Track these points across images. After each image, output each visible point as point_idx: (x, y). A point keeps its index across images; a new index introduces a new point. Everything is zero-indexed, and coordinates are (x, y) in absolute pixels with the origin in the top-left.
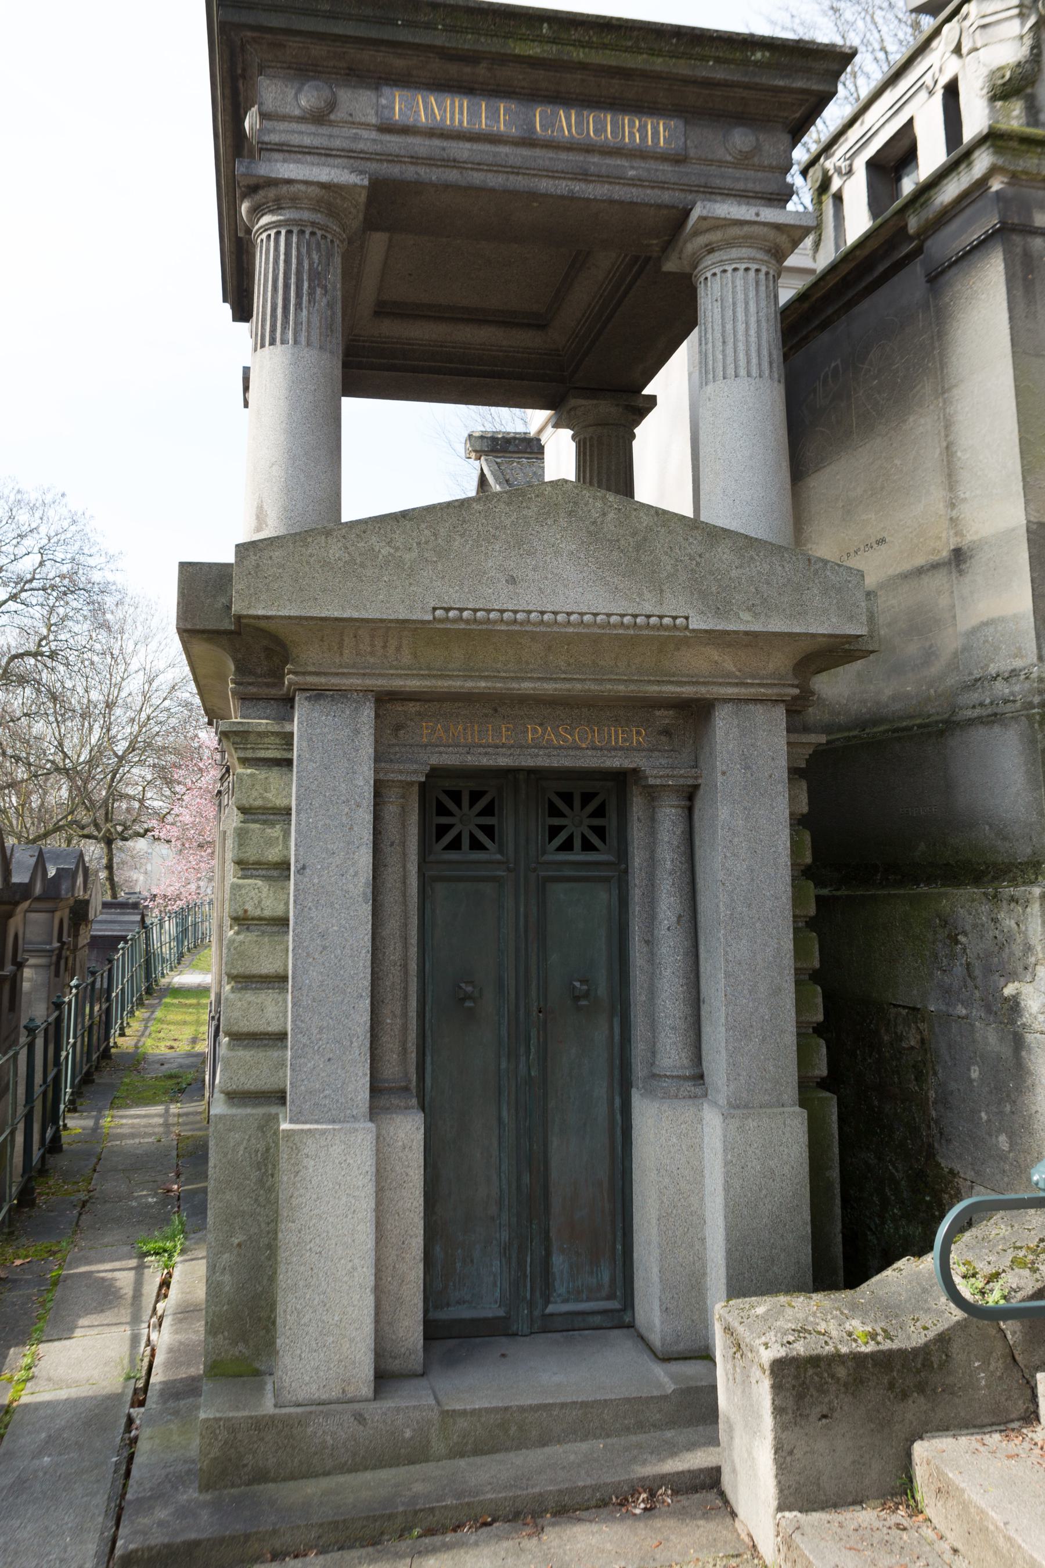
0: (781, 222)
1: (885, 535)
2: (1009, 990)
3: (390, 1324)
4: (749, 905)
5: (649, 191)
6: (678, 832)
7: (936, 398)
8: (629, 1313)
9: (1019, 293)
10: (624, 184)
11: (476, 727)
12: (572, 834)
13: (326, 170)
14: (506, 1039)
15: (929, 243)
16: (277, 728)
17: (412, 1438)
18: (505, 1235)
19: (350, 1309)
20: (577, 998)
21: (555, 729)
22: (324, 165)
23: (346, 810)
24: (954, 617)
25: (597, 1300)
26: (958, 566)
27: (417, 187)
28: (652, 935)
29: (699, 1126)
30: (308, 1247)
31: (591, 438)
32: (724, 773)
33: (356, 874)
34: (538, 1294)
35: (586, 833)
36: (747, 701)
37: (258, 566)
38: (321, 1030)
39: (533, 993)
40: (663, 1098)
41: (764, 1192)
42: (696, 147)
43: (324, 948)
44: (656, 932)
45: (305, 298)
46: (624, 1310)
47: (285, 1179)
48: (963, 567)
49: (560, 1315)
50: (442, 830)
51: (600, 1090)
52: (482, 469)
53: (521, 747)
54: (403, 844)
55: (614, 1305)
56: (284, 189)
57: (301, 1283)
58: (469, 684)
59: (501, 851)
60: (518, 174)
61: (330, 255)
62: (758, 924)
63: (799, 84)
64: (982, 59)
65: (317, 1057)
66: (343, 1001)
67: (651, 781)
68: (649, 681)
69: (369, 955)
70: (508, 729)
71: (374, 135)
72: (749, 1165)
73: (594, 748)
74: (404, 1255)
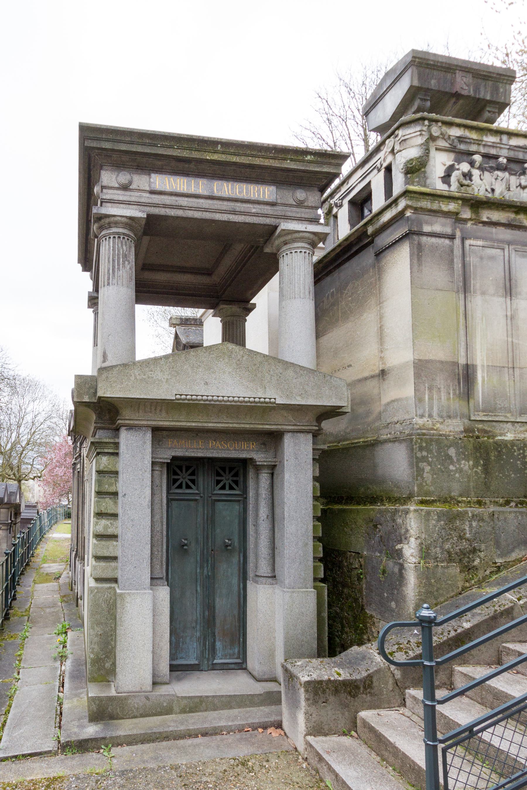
0: (316, 231)
1: (351, 363)
2: (399, 547)
5: (261, 218)
6: (268, 483)
7: (377, 306)
8: (245, 664)
9: (415, 261)
10: (250, 215)
13: (129, 211)
15: (376, 239)
16: (112, 441)
17: (166, 706)
18: (198, 634)
19: (143, 659)
22: (128, 209)
24: (380, 398)
25: (233, 659)
26: (383, 377)
27: (165, 218)
28: (257, 522)
31: (229, 321)
32: (287, 461)
33: (145, 497)
34: (211, 656)
37: (107, 377)
38: (132, 555)
39: (210, 544)
42: (281, 198)
43: (133, 525)
45: (121, 266)
46: (243, 663)
47: (119, 610)
48: (385, 377)
49: (219, 664)
50: (175, 481)
51: (235, 581)
52: (176, 332)
53: (207, 449)
54: (161, 486)
55: (239, 661)
56: (112, 219)
57: (125, 649)
58: (189, 424)
59: (197, 489)
60: (207, 211)
61: (130, 247)
62: (299, 520)
63: (325, 170)
64: (403, 155)
67: (258, 463)
68: (259, 424)
70: (202, 442)
71: (148, 195)
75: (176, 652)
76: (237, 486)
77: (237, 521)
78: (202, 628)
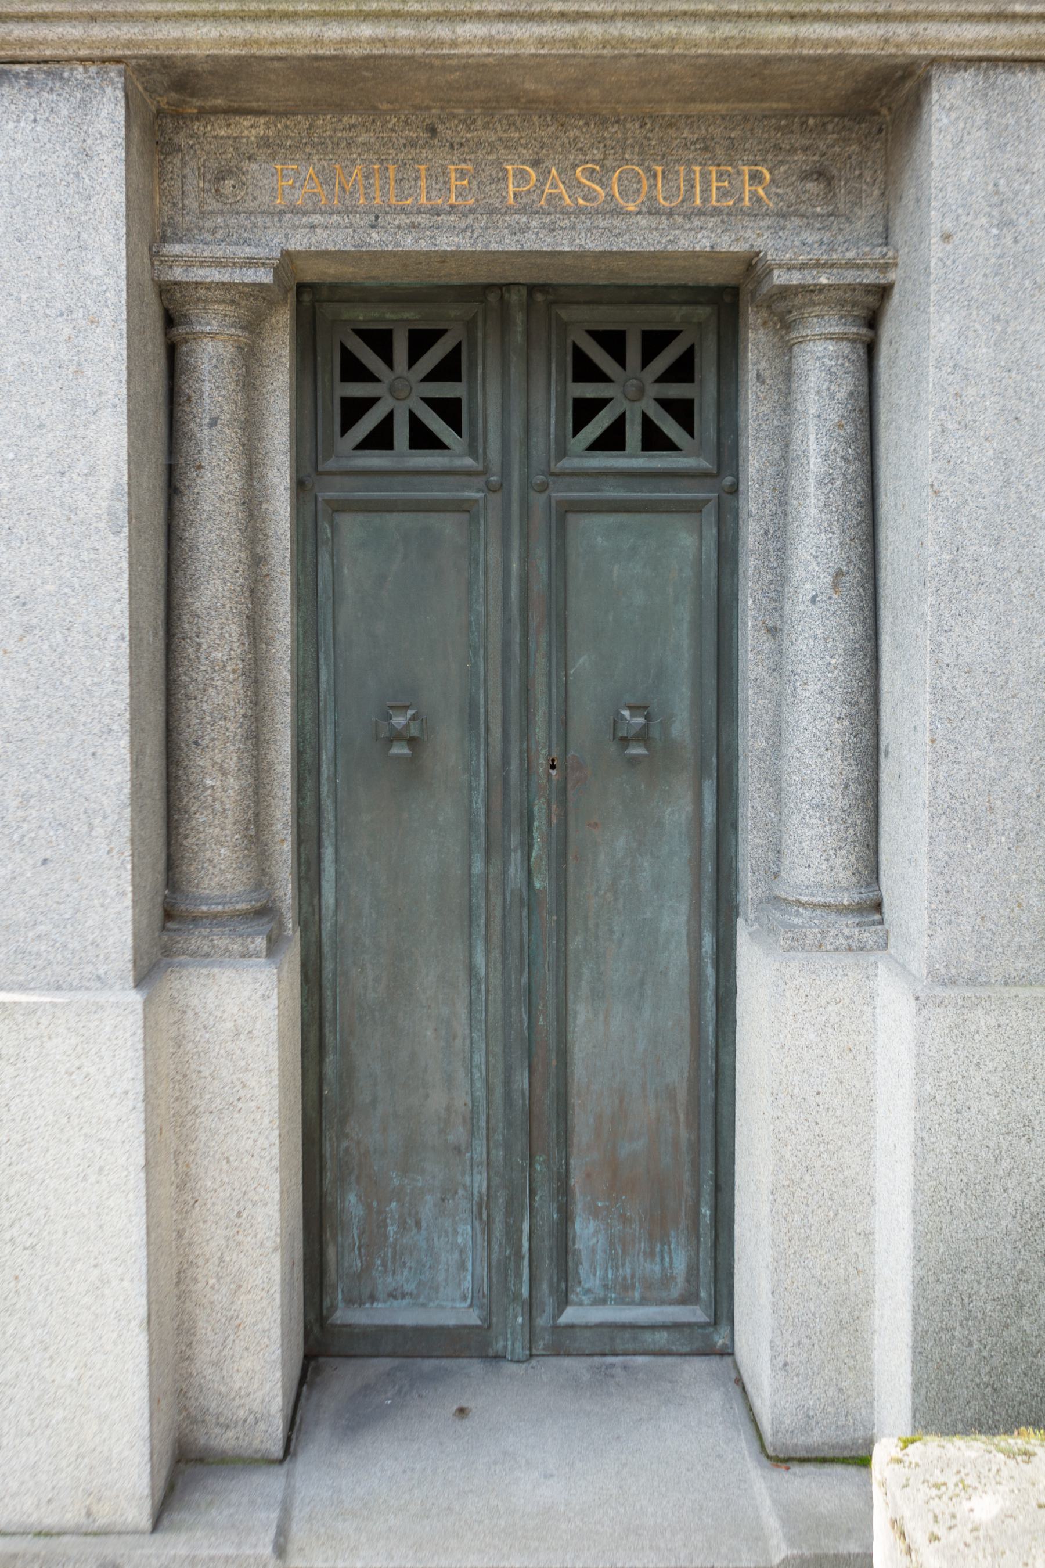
3: (215, 1364)
4: (998, 541)
6: (842, 394)
8: (724, 1330)
11: (392, 173)
12: (623, 415)
14: (482, 819)
18: (479, 1182)
20: (625, 741)
21: (567, 171)
23: (68, 331)
25: (662, 1302)
29: (868, 1010)
30: (7, 1236)
32: (947, 237)
33: (92, 470)
34: (545, 1287)
35: (651, 414)
36: (1013, 63)
38: (25, 800)
39: (539, 732)
40: (791, 948)
41: (1006, 1164)
43: (28, 629)
44: (787, 608)
53: (492, 212)
59: (472, 451)
62: (1017, 586)
65: (18, 856)
66: (70, 740)
67: (779, 278)
69: (125, 646)
70: (462, 174)
72: (975, 1106)
73: (654, 212)
74: (240, 1238)
75: (368, 1267)
76: (690, 430)
77: (684, 612)
78: (498, 1154)
